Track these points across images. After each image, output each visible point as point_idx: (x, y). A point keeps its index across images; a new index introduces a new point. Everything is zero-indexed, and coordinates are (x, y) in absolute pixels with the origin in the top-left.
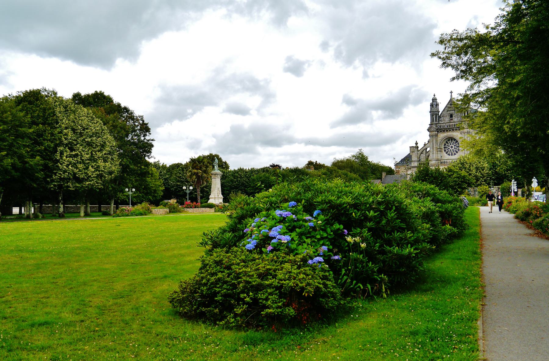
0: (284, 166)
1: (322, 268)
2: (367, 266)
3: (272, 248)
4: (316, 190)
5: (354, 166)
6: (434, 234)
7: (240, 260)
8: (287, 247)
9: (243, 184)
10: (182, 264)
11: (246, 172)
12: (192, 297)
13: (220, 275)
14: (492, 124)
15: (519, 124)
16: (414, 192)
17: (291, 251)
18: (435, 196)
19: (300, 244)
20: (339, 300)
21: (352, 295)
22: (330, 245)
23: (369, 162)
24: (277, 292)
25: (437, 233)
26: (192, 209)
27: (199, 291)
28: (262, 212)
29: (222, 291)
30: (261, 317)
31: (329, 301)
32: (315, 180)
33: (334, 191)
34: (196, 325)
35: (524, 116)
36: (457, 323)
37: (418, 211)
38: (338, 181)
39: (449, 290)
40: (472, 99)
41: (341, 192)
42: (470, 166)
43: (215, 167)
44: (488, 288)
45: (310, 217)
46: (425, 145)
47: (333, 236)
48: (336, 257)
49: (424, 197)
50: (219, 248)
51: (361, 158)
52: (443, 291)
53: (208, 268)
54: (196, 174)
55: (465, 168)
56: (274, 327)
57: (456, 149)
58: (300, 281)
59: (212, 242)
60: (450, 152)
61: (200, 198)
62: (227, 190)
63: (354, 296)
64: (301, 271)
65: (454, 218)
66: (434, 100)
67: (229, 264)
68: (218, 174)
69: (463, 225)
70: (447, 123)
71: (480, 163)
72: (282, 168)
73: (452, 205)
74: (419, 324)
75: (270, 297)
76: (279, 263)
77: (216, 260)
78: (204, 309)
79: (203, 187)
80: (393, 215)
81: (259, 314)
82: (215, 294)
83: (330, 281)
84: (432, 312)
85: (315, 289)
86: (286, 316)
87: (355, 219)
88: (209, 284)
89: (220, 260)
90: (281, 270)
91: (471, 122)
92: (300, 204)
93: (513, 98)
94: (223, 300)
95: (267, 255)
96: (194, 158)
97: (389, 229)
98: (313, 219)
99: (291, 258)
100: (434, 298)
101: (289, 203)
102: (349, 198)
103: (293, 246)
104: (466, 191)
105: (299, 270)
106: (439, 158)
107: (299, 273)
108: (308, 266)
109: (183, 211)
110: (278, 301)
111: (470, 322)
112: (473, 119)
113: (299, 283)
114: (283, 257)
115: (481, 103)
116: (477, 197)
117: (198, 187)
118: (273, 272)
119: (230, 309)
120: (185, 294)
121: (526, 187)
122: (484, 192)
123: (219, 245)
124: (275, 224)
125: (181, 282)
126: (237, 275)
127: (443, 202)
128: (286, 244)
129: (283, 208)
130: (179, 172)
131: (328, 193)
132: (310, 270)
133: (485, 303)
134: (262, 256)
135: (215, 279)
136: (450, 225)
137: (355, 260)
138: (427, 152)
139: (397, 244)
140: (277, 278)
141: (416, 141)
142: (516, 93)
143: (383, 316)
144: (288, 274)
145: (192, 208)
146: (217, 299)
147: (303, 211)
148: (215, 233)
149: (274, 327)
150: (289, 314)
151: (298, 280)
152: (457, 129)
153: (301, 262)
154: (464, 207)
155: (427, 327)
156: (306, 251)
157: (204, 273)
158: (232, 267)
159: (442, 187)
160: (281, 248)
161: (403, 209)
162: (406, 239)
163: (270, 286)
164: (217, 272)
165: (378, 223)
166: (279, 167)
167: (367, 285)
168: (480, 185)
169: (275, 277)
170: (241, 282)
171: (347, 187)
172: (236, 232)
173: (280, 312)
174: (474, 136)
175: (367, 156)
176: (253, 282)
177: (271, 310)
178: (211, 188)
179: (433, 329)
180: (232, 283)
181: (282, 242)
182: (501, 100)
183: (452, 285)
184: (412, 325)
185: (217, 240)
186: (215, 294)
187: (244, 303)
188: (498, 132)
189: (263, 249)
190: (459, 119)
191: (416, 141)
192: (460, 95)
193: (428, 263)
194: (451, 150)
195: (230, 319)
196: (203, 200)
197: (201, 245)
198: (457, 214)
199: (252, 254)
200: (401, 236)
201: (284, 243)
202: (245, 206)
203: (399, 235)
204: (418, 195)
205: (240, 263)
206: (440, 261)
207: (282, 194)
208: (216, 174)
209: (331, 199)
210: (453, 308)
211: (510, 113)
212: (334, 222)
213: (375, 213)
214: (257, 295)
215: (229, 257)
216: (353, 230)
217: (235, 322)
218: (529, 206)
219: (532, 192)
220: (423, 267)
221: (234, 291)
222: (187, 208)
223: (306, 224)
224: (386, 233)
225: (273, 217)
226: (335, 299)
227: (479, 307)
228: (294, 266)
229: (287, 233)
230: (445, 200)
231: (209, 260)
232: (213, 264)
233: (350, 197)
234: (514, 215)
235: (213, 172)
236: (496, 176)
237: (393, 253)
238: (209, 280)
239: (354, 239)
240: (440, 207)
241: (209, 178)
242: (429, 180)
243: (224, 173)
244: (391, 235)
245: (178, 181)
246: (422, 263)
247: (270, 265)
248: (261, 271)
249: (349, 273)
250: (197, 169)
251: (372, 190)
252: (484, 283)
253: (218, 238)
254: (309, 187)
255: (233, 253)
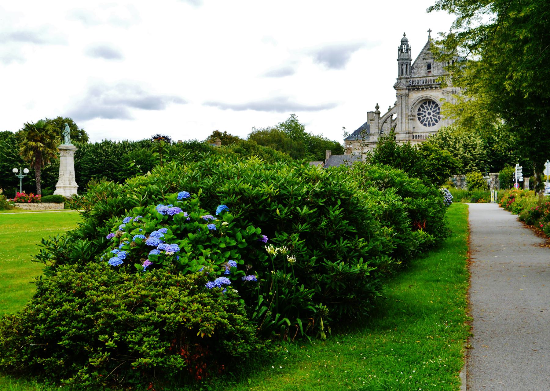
0: (175, 138)
1: (228, 295)
2: (297, 290)
3: (149, 263)
4: (221, 173)
5: (284, 140)
6: (399, 244)
7: (99, 282)
8: (174, 262)
9: (110, 166)
10: (7, 289)
11: (115, 147)
12: (21, 341)
13: (67, 306)
14: (487, 79)
15: (526, 80)
16: (372, 180)
17: (179, 268)
18: (402, 186)
19: (194, 258)
20: (254, 342)
21: (274, 335)
22: (242, 259)
23: (306, 134)
24: (157, 331)
25: (404, 242)
26: (26, 204)
27: (33, 331)
28: (135, 206)
29: (71, 330)
30: (131, 371)
31: (238, 345)
32: (220, 158)
33: (248, 176)
34: (27, 385)
35: (533, 68)
36: (430, 375)
37: (376, 209)
38: (255, 161)
39: (419, 327)
40: (459, 42)
41: (259, 178)
42: (455, 143)
43: (66, 138)
44: (477, 324)
45: (210, 215)
46: (390, 109)
47: (246, 245)
48: (251, 278)
49: (386, 188)
50: (67, 264)
51: (294, 128)
52: (411, 328)
53: (48, 296)
54: (35, 149)
55: (449, 146)
56: (151, 387)
57: (436, 116)
58: (193, 314)
59: (56, 255)
60: (426, 121)
61: (41, 188)
62: (84, 176)
63: (278, 337)
64: (195, 298)
65: (429, 219)
66: (404, 42)
67: (82, 289)
68: (70, 150)
69: (444, 231)
70: (422, 77)
71: (469, 138)
72: (172, 142)
73: (428, 200)
74: (373, 378)
75: (145, 339)
76: (161, 287)
77: (60, 283)
78: (39, 360)
79: (46, 170)
80: (337, 212)
81: (129, 367)
82: (59, 336)
83: (239, 313)
84: (393, 359)
85: (216, 326)
86: (171, 368)
87: (280, 218)
88: (49, 320)
89: (67, 283)
90: (163, 297)
91: (456, 76)
92: (195, 195)
93: (519, 40)
94: (72, 346)
95: (142, 275)
96: (31, 123)
97: (331, 234)
98: (216, 219)
99: (179, 279)
100: (396, 338)
101: (179, 194)
102: (271, 186)
103: (184, 260)
104: (450, 180)
105: (191, 297)
106: (411, 129)
107: (192, 302)
108: (206, 291)
109: (12, 207)
110: (159, 345)
111: (448, 373)
112: (459, 71)
113: (191, 317)
114: (167, 277)
115: (472, 47)
116: (466, 189)
117: (38, 169)
118: (151, 301)
119: (83, 359)
120: (10, 336)
121: (535, 175)
122: (475, 182)
123: (68, 260)
124: (156, 226)
125: (4, 318)
126: (94, 306)
127: (415, 195)
128: (172, 258)
129: (168, 202)
130: (7, 146)
131: (238, 179)
132: (208, 297)
133: (471, 346)
134: (134, 276)
135: (58, 312)
136: (424, 230)
137: (279, 281)
138: (392, 121)
139: (343, 257)
140: (157, 309)
141: (377, 104)
142: (522, 34)
143: (320, 366)
144: (174, 303)
145: (27, 202)
146: (61, 343)
147: (201, 207)
148: (61, 240)
149: (151, 387)
150: (175, 366)
151: (189, 313)
152: (438, 86)
153: (195, 284)
154: (446, 204)
155: (385, 381)
156: (204, 268)
157: (41, 304)
158: (86, 293)
159: (414, 173)
160: (165, 263)
161: (353, 203)
162: (356, 250)
163: (145, 322)
164: (62, 300)
165: (316, 224)
166: (166, 139)
167: (297, 321)
168: (470, 171)
169: (153, 308)
170: (100, 317)
171: (269, 170)
172: (94, 238)
173: (162, 362)
174: (461, 97)
175: (303, 124)
176: (119, 317)
177: (147, 360)
178: (58, 171)
179: (394, 385)
180: (87, 318)
181: (167, 253)
182: (501, 43)
183: (424, 319)
184: (363, 379)
185: (65, 251)
186: (59, 336)
187: (105, 349)
188: (496, 91)
189: (136, 265)
190: (441, 71)
191: (377, 104)
192: (442, 34)
193: (390, 287)
194: (428, 118)
195: (82, 374)
196: (45, 191)
197: (37, 259)
198: (435, 214)
199: (119, 273)
200: (348, 245)
201: (169, 255)
202: (110, 198)
203: (347, 243)
204: (378, 184)
205: (99, 286)
206: (408, 284)
207: (167, 180)
208: (66, 150)
209: (243, 187)
210: (424, 354)
211: (514, 63)
212: (248, 223)
213: (310, 210)
214: (125, 336)
215: (81, 278)
216: (277, 235)
217: (90, 379)
218: (539, 202)
219: (545, 183)
220: (381, 292)
221: (90, 330)
222: (20, 202)
223: (204, 226)
224: (327, 240)
225: (152, 214)
226: (247, 342)
227: (463, 352)
228: (184, 290)
229: (173, 239)
230: (417, 193)
231: (50, 282)
232: (56, 288)
233: (272, 184)
234: (517, 216)
235: (62, 146)
236: (493, 159)
237: (337, 272)
238: (48, 314)
239: (277, 249)
240: (409, 203)
241: (56, 156)
242: (394, 161)
243: (80, 148)
244: (335, 243)
245: (6, 160)
246: (381, 286)
247: (147, 290)
248: (132, 299)
249: (270, 301)
250: (36, 141)
251: (306, 174)
252: (471, 316)
253: (66, 248)
254: (209, 170)
255: (89, 271)
